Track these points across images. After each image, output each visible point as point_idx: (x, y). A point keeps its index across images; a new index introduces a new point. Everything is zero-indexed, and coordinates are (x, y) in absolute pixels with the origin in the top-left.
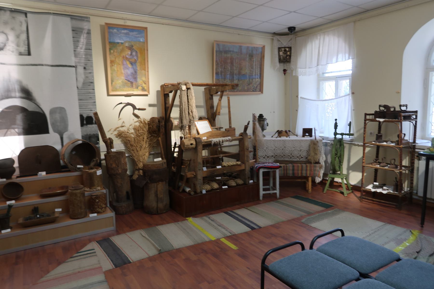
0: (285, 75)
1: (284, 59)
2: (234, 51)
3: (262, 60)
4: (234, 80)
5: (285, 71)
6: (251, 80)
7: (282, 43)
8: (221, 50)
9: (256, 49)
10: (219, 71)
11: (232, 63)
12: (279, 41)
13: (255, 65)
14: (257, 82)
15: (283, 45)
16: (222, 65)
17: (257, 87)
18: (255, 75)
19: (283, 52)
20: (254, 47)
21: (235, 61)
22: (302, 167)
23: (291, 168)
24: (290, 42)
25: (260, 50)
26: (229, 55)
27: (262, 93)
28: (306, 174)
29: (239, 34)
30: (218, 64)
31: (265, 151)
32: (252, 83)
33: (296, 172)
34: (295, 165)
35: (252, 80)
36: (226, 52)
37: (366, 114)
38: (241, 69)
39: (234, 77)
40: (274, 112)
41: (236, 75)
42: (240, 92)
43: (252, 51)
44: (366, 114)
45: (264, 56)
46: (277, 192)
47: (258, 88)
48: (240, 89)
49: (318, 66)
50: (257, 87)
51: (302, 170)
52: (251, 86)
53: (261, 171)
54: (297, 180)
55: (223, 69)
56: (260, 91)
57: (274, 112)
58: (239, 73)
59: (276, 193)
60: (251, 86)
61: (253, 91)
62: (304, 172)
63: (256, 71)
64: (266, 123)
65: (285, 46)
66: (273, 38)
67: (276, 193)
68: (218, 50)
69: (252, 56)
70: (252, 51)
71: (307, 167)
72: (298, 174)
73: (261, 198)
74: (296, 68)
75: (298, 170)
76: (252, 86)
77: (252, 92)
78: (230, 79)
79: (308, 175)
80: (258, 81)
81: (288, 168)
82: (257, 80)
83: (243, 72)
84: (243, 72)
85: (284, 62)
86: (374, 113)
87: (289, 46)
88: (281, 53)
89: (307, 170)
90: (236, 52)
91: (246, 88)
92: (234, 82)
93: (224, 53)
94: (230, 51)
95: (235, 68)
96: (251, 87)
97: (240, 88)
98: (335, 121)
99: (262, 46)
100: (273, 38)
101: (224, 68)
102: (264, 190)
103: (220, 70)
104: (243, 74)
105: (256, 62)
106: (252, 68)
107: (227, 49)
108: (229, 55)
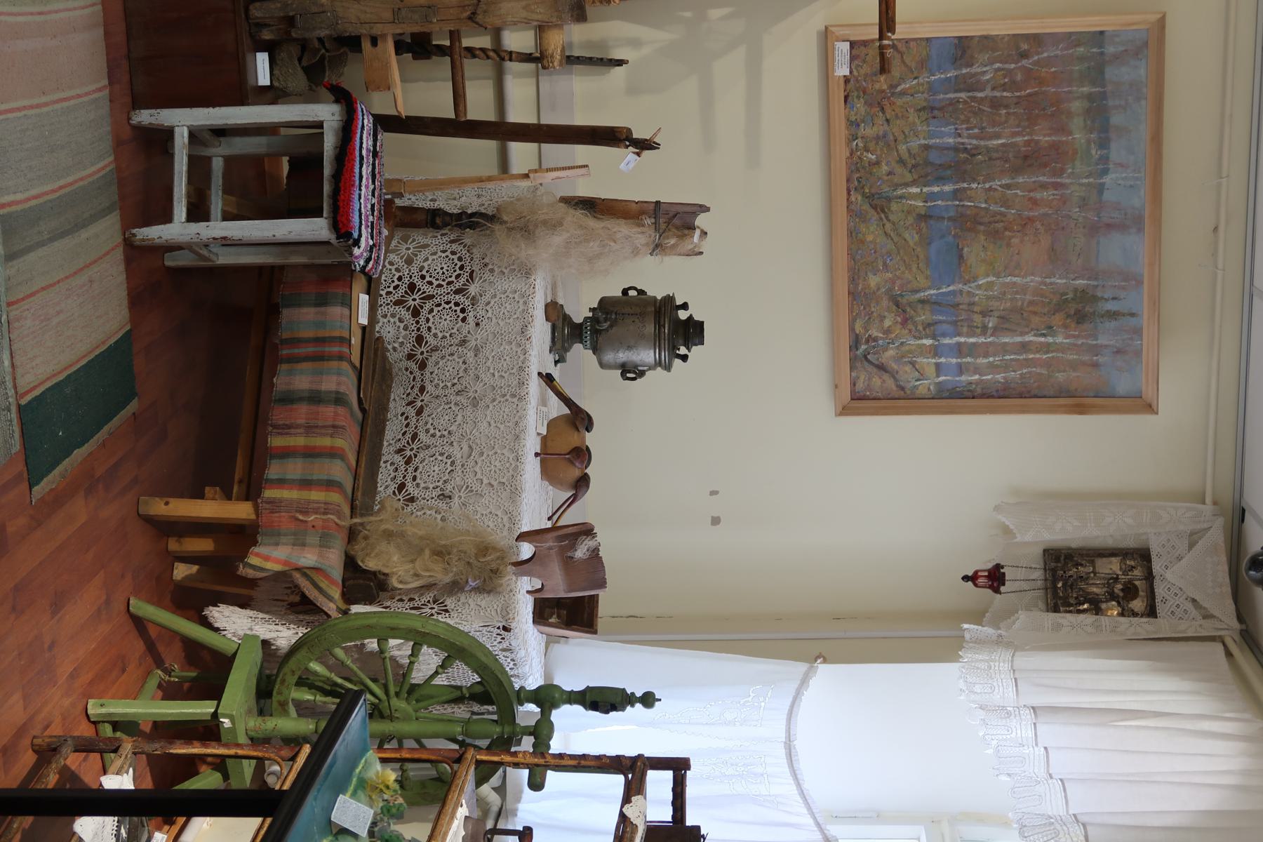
0: (966, 578)
1: (1071, 587)
2: (1105, 172)
3: (1062, 401)
4: (922, 180)
5: (995, 578)
6: (924, 316)
7: (1180, 558)
8: (1110, 73)
9: (1128, 353)
10: (976, 69)
11: (1029, 159)
12: (1191, 545)
13: (1024, 347)
14: (913, 364)
15: (1167, 567)
16: (1013, 86)
17: (882, 368)
18: (959, 350)
19: (1116, 579)
20: (1138, 332)
21: (1044, 186)
22: (333, 453)
23: (329, 384)
24: (1189, 606)
25: (1123, 385)
26: (1078, 135)
27: (844, 411)
28: (281, 483)
29: (1216, 229)
30: (1024, 55)
31: (458, 292)
32: (904, 323)
33: (302, 413)
34: (348, 419)
35: (930, 329)
36: (1098, 112)
37: (679, 767)
38: (996, 230)
39: (941, 180)
40: (716, 521)
41: (956, 194)
42: (850, 233)
43: (1114, 315)
44: (679, 767)
45: (1081, 409)
46: (178, 229)
47: (879, 383)
48: (870, 238)
49: (1028, 715)
50: (882, 368)
51: (310, 454)
52: (887, 323)
53: (327, 113)
54: (239, 453)
55: (988, 93)
56: (856, 397)
57: (716, 521)
58: (967, 222)
59: (167, 218)
60: (887, 323)
61: (855, 343)
62: (294, 469)
63: (986, 355)
64: (646, 355)
65: (1157, 582)
66: (1208, 500)
67: (167, 218)
68: (1110, 49)
69: (1080, 318)
70: (1114, 315)
71: (330, 485)
72: (285, 429)
73: (145, 117)
74: (1014, 646)
75: (310, 429)
76: (887, 332)
77: (852, 329)
78: (927, 148)
79: (268, 493)
80: (922, 376)
81: (334, 364)
82: (927, 363)
83: (975, 251)
84: (975, 251)
85: (1055, 588)
86: (690, 821)
87: (1164, 601)
88: (1112, 566)
89: (306, 484)
90: (1101, 189)
91: (874, 280)
92: (914, 183)
93: (1090, 97)
94: (1104, 144)
95: (996, 184)
96: (882, 318)
97: (872, 233)
98: (638, 694)
99: (1148, 394)
100: (1208, 500)
101: (995, 104)
102: (198, 212)
103: (984, 69)
104: (961, 257)
105: (1047, 348)
106: (1006, 323)
107: (1116, 119)
108: (1078, 135)
